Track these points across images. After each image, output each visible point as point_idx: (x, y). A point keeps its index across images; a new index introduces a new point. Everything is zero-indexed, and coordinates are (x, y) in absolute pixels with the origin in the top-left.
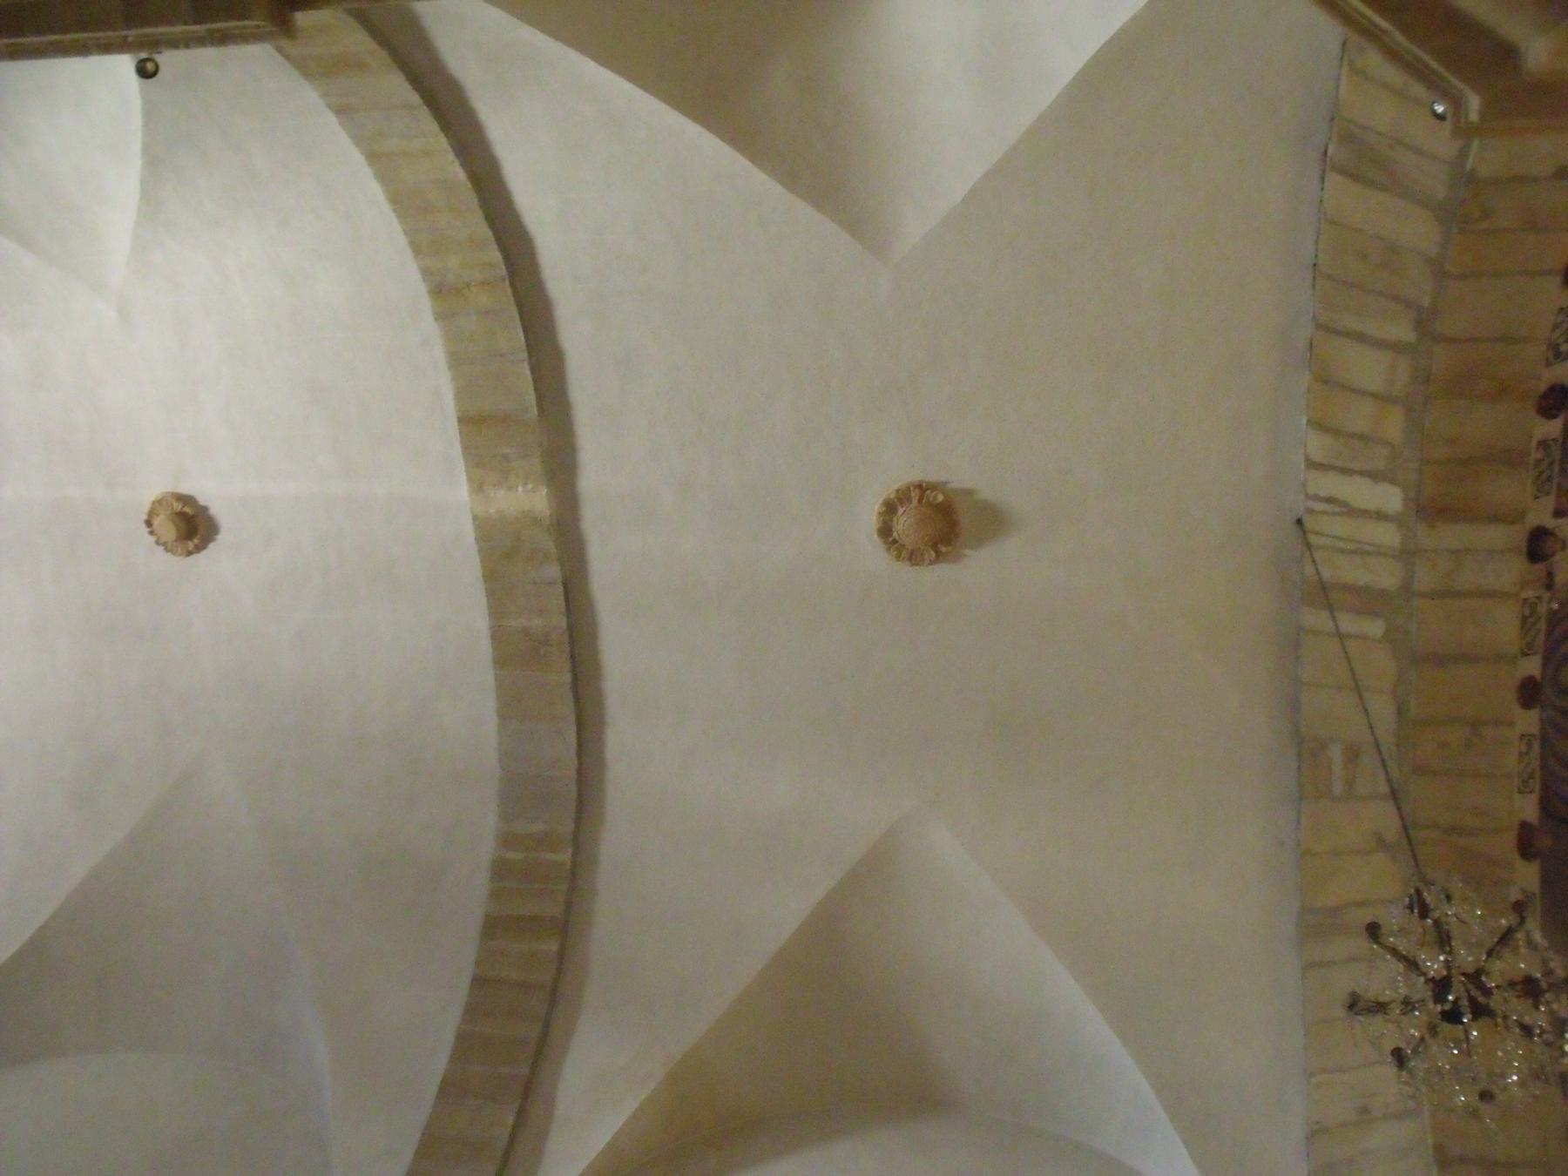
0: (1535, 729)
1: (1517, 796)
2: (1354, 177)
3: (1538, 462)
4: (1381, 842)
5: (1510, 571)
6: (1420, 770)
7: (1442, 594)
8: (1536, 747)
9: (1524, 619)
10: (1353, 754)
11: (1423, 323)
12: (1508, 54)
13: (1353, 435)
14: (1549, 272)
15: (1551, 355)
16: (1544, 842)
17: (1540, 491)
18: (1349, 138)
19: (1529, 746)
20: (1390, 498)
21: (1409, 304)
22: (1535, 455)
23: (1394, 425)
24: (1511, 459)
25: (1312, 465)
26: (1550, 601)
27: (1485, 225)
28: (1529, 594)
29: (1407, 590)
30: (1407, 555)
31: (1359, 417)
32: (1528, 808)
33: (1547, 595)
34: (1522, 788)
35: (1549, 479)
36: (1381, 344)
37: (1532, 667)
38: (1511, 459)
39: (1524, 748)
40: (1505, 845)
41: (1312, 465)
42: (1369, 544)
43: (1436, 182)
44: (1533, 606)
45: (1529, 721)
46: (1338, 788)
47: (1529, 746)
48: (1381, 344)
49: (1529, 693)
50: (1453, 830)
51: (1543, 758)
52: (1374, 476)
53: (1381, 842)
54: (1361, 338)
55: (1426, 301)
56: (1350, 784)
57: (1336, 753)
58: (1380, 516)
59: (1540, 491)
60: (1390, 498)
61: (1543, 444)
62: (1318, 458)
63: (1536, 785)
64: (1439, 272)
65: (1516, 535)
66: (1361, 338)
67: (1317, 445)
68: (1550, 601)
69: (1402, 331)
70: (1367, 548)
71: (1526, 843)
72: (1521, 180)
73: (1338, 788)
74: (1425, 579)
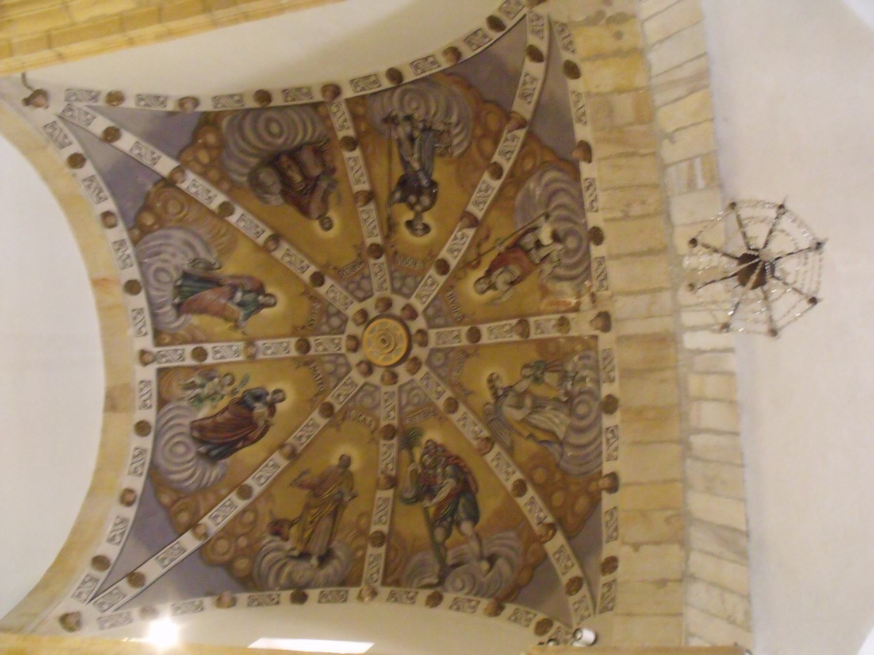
2: (735, 530)
3: (612, 370)
5: (620, 308)
6: (656, 186)
7: (655, 291)
8: (587, 205)
9: (605, 278)
10: (691, 185)
13: (715, 373)
14: (628, 484)
16: (576, 154)
17: (608, 356)
18: (743, 556)
20: (691, 341)
21: (697, 458)
23: (694, 384)
24: (628, 373)
25: (730, 350)
26: (591, 286)
27: (669, 513)
29: (674, 289)
30: (677, 310)
31: (712, 385)
32: (587, 170)
35: (605, 359)
36: (708, 431)
37: (597, 251)
38: (628, 373)
41: (730, 350)
43: (698, 537)
44: (601, 286)
45: (594, 219)
46: (698, 162)
47: (592, 207)
48: (708, 431)
49: (597, 236)
50: (634, 154)
52: (700, 352)
53: (671, 137)
54: (717, 432)
56: (691, 167)
57: (701, 183)
61: (612, 381)
62: (730, 355)
63: (584, 185)
64: (685, 483)
66: (717, 432)
67: (732, 363)
68: (591, 286)
69: (697, 441)
70: (699, 308)
71: (586, 150)
72: (657, 543)
73: (698, 162)
74: (666, 298)
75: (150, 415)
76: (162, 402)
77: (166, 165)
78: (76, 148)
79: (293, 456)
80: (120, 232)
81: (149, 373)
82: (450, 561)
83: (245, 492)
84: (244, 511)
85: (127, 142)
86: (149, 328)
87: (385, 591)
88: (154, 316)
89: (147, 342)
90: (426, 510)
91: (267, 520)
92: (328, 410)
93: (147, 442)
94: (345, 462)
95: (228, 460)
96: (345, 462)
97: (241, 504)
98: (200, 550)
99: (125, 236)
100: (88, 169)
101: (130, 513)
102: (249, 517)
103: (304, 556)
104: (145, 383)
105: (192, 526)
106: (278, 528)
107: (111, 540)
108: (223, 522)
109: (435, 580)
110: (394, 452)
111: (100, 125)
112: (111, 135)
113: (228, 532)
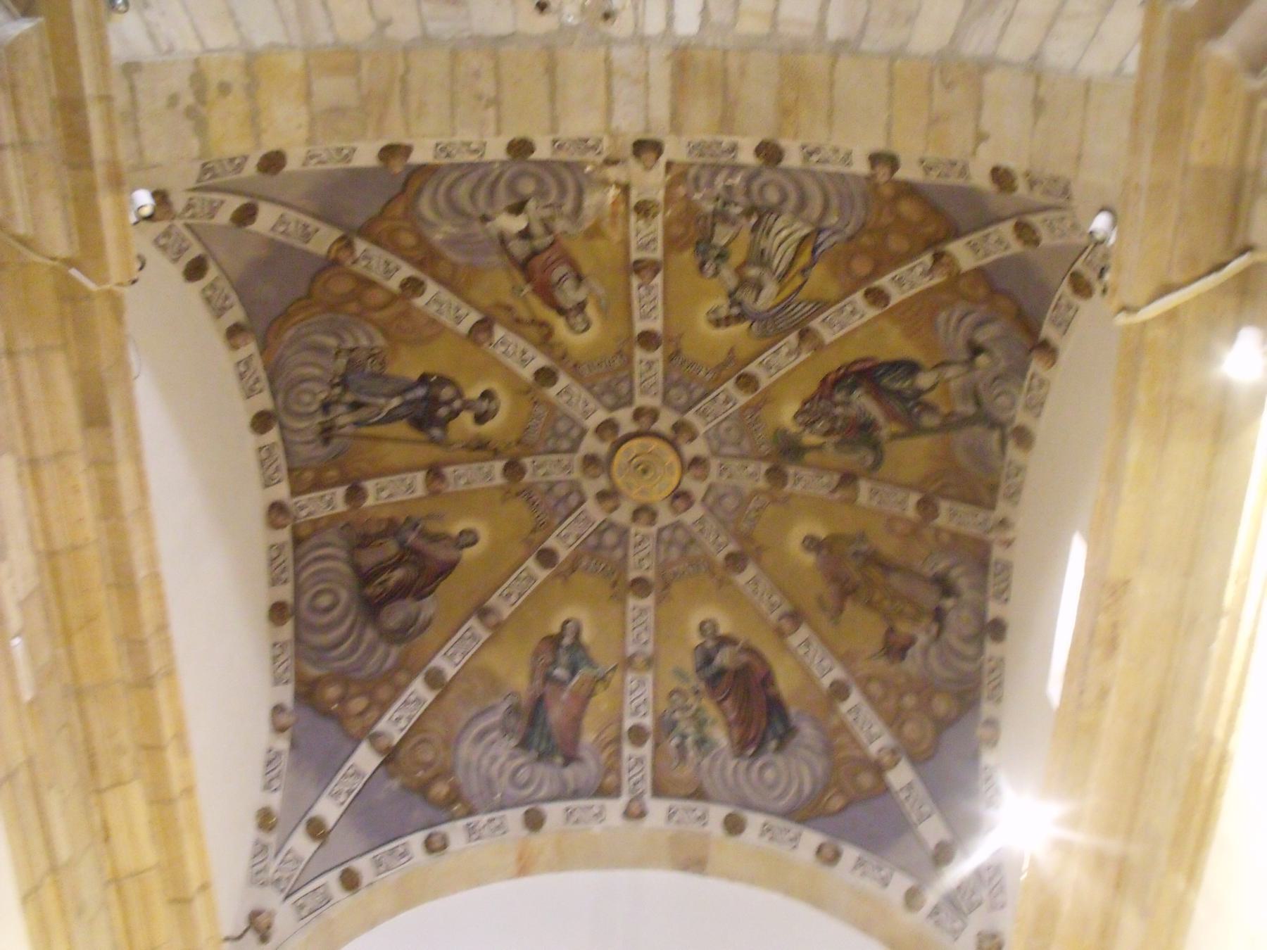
0: (489, 156)
1: (434, 142)
4: (384, 24)
5: (630, 125)
6: (454, 55)
8: (473, 158)
11: (840, 48)
12: (1217, 27)
15: (810, 148)
16: (397, 167)
19: (476, 151)
20: (687, 25)
21: (862, 32)
22: (726, 140)
23: (751, 25)
28: (606, 143)
30: (640, 39)
32: (422, 155)
33: (600, 159)
34: (439, 147)
37: (542, 151)
39: (473, 146)
40: (396, 135)
42: (644, 10)
43: (976, 45)
44: (594, 148)
45: (496, 151)
49: (520, 148)
51: (459, 166)
55: (865, 46)
58: (670, 19)
59: (694, 148)
60: (687, 25)
63: (443, 161)
64: (893, 56)
65: (660, 132)
69: (836, 29)
72: (979, 107)
74: (623, 56)
75: (718, 813)
76: (699, 794)
77: (366, 759)
78: (332, 879)
79: (796, 617)
80: (455, 831)
81: (657, 809)
82: (968, 409)
83: (840, 691)
84: (869, 698)
85: (329, 810)
86: (596, 803)
87: (1002, 508)
88: (576, 794)
89: (614, 808)
90: (894, 437)
91: (881, 664)
92: (736, 561)
93: (755, 821)
94: (812, 544)
95: (793, 710)
96: (812, 544)
97: (855, 698)
98: (917, 761)
99: (461, 823)
100: (363, 865)
101: (850, 854)
102: (875, 688)
103: (939, 615)
104: (671, 814)
105: (878, 769)
106: (896, 649)
107: (885, 883)
108: (878, 727)
109: (995, 436)
110: (806, 473)
111: (302, 844)
112: (317, 830)
113: (894, 720)
